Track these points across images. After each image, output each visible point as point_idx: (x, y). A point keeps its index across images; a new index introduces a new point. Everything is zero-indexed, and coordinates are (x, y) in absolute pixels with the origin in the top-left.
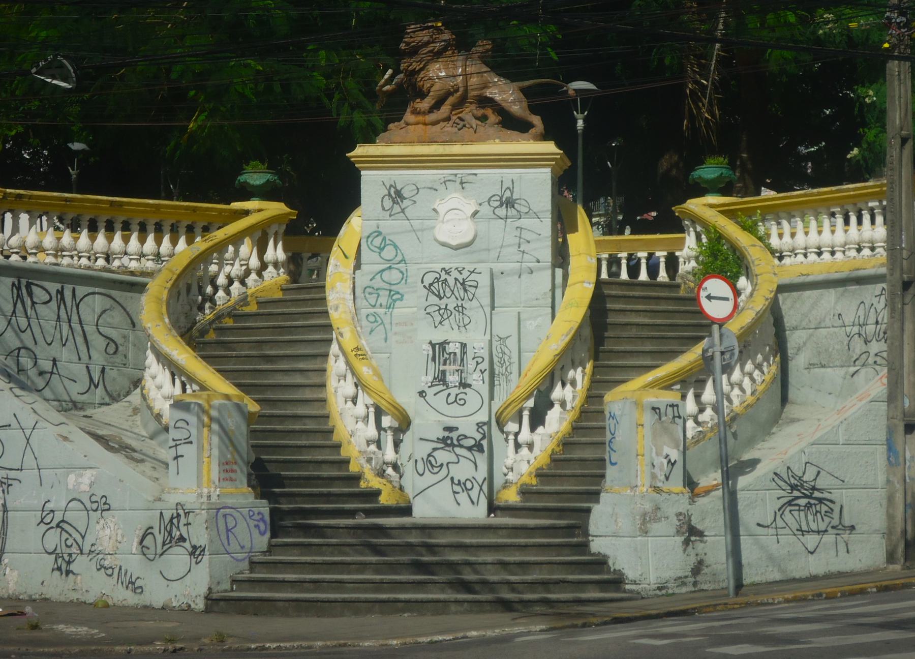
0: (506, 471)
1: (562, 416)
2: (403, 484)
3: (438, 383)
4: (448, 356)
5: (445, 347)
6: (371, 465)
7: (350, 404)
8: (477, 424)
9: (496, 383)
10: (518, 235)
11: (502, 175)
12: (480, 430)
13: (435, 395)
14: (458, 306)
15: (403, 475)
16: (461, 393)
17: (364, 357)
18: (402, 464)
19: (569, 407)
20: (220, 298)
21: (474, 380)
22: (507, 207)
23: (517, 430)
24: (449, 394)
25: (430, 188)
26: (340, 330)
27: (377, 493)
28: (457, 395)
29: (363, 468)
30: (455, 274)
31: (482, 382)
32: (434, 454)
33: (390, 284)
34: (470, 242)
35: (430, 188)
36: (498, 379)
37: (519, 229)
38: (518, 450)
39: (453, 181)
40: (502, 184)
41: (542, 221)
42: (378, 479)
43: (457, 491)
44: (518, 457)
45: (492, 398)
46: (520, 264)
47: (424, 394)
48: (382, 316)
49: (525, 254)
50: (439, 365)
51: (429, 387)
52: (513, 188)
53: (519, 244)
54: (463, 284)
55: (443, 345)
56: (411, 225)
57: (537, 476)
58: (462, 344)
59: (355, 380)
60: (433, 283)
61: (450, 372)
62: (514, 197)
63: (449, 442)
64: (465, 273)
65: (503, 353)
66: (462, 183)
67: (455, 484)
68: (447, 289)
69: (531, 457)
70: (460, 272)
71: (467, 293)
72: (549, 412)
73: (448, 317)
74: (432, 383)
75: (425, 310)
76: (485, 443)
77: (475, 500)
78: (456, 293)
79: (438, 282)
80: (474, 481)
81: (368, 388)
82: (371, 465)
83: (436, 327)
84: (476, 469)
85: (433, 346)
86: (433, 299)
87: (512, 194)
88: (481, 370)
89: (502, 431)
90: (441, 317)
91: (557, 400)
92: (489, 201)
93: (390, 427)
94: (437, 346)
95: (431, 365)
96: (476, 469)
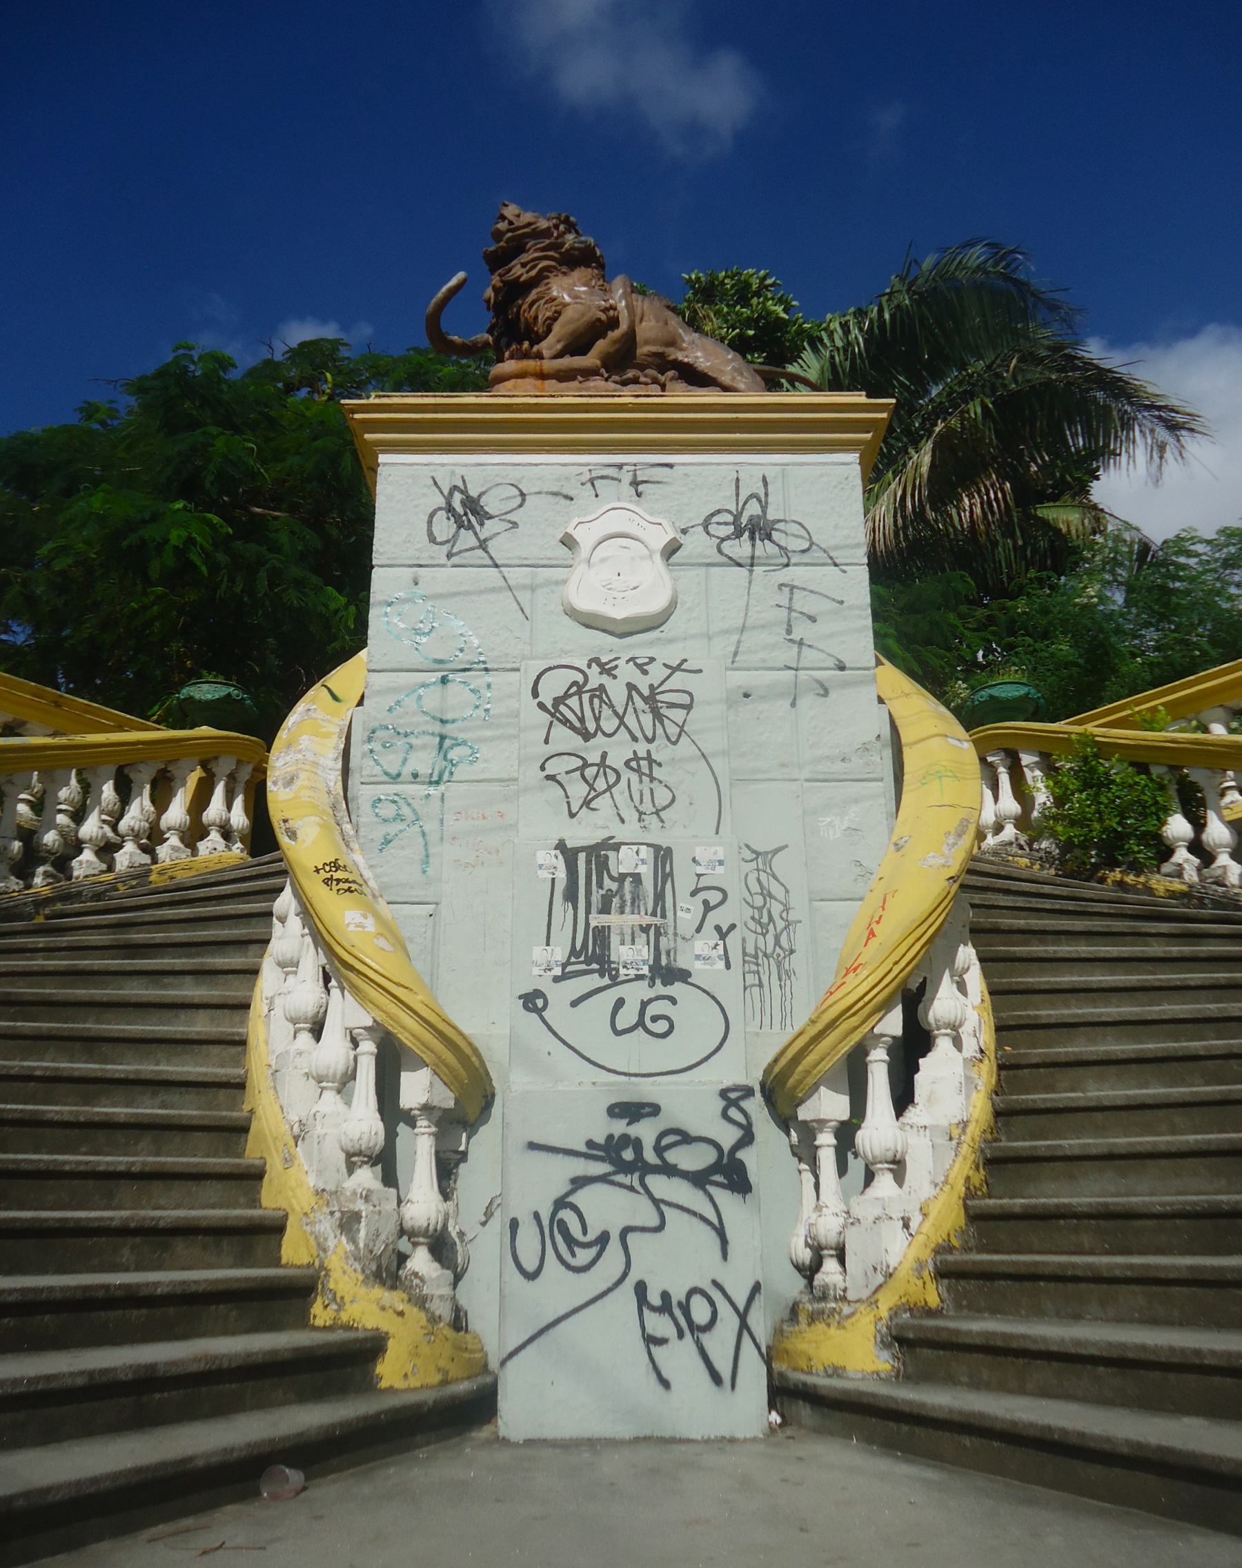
2: (463, 1302)
3: (583, 967)
4: (614, 886)
5: (607, 857)
6: (353, 1240)
7: (305, 1038)
8: (724, 1093)
10: (785, 603)
12: (734, 1113)
13: (574, 1004)
14: (636, 758)
15: (465, 1270)
17: (354, 886)
18: (461, 1234)
20: (81, 863)
21: (698, 957)
22: (752, 538)
23: (845, 1115)
24: (620, 1003)
26: (291, 824)
27: (373, 1347)
29: (325, 1250)
30: (627, 673)
31: (721, 964)
32: (578, 1199)
33: (442, 721)
37: (786, 590)
39: (613, 479)
40: (737, 487)
41: (844, 572)
42: (378, 1292)
43: (659, 1334)
44: (865, 1207)
46: (793, 672)
47: (540, 1003)
48: (415, 804)
49: (804, 648)
50: (588, 912)
51: (557, 979)
52: (766, 494)
53: (789, 625)
54: (651, 700)
55: (600, 853)
56: (504, 577)
57: (943, 1273)
58: (657, 848)
59: (323, 960)
60: (567, 695)
61: (622, 934)
62: (772, 515)
63: (628, 1155)
64: (657, 673)
65: (767, 895)
66: (635, 483)
67: (653, 1309)
68: (607, 712)
72: (916, 1076)
73: (609, 788)
74: (564, 966)
75: (543, 768)
78: (630, 720)
79: (579, 693)
80: (716, 1295)
81: (359, 973)
82: (353, 1240)
83: (572, 815)
85: (569, 854)
86: (564, 738)
87: (764, 509)
89: (785, 1121)
93: (427, 1108)
94: (582, 857)
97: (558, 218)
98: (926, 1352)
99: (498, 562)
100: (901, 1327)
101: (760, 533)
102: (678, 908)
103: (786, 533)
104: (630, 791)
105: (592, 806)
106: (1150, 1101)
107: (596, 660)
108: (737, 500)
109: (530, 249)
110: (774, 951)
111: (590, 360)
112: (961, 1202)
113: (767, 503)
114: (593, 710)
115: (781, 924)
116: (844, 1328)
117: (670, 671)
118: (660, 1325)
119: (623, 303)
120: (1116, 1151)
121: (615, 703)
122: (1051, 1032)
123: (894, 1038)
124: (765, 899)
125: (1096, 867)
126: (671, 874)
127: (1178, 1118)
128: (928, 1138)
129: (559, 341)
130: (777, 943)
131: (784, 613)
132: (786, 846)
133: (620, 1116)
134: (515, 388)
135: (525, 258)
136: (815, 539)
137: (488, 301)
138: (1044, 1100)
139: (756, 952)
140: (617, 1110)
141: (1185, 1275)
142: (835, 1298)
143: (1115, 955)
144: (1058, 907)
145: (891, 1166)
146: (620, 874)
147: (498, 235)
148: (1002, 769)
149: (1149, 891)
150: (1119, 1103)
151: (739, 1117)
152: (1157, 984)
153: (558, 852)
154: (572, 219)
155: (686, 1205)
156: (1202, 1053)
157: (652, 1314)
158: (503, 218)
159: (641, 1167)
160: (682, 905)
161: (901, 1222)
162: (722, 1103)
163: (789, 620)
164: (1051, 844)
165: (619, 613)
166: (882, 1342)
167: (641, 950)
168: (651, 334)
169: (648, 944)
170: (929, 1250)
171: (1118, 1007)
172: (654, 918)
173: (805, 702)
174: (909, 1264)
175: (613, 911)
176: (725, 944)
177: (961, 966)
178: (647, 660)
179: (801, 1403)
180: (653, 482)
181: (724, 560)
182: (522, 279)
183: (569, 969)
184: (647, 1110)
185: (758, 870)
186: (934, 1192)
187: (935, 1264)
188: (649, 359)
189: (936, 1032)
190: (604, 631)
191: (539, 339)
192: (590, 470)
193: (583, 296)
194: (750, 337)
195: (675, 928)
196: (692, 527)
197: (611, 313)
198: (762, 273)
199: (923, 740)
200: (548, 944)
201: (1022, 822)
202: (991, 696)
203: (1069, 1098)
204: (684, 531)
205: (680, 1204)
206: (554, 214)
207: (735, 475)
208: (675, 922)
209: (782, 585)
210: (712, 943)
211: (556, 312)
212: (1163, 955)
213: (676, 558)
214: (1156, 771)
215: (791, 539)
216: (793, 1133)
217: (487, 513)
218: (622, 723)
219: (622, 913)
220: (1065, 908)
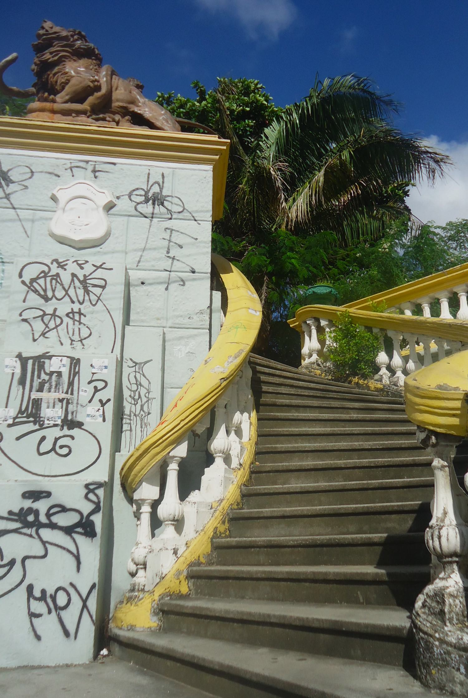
0: (133, 568)
1: (227, 475)
3: (25, 419)
4: (47, 378)
5: (44, 362)
8: (87, 486)
9: (125, 427)
10: (168, 238)
11: (149, 168)
12: (91, 496)
13: (18, 439)
14: (73, 312)
16: (64, 436)
19: (235, 463)
21: (88, 415)
22: (154, 204)
23: (156, 497)
24: (43, 439)
25: (50, 173)
28: (56, 440)
30: (72, 268)
31: (101, 419)
34: (101, 238)
35: (50, 173)
36: (128, 421)
37: (169, 231)
38: (156, 532)
39: (83, 168)
40: (148, 177)
41: (199, 224)
43: (37, 612)
44: (157, 543)
45: (116, 447)
46: (169, 272)
50: (31, 391)
51: (9, 426)
52: (163, 182)
54: (84, 283)
57: (191, 576)
58: (72, 359)
60: (38, 278)
61: (48, 403)
62: (164, 193)
64: (88, 269)
66: (94, 171)
67: (36, 599)
68: (59, 287)
69: (179, 541)
70: (81, 266)
71: (88, 294)
72: (202, 477)
73: (56, 327)
74: (14, 419)
76: (97, 519)
77: (71, 629)
78: (71, 292)
79: (45, 277)
83: (35, 340)
84: (78, 569)
85: (23, 361)
86: (34, 299)
87: (161, 189)
88: (101, 401)
89: (131, 500)
90: (44, 326)
91: (220, 452)
92: (130, 195)
94: (30, 362)
95: (16, 390)
96: (78, 569)
97: (74, 32)
98: (172, 617)
99: (15, 206)
100: (162, 605)
101: (158, 202)
102: (80, 390)
103: (172, 203)
104: (67, 329)
105: (46, 336)
106: (311, 490)
107: (56, 261)
108: (148, 184)
109: (55, 45)
110: (140, 413)
111: (86, 106)
112: (210, 540)
113: (163, 187)
114: (52, 286)
115: (144, 399)
116: (137, 605)
117: (96, 268)
118: (38, 607)
119: (105, 79)
120: (286, 514)
121: (64, 283)
122: (283, 455)
123: (182, 458)
124: (138, 387)
125: (348, 376)
126: (78, 372)
127: (323, 497)
128: (196, 508)
129: (67, 95)
130: (142, 409)
131: (166, 243)
132: (152, 360)
133: (29, 498)
134: (37, 116)
135: (53, 49)
136: (186, 207)
137: (33, 70)
138: (264, 489)
139: (130, 413)
140: (27, 495)
141: (285, 576)
142: (138, 590)
143: (326, 418)
144: (312, 394)
145: (173, 523)
146: (51, 372)
147: (39, 36)
148: (313, 327)
149: (368, 388)
150: (298, 490)
151: (94, 498)
152: (339, 432)
153: (17, 359)
154: (83, 33)
155: (60, 544)
156: (343, 466)
157: (35, 601)
158: (43, 28)
159: (38, 525)
160: (83, 388)
161: (173, 551)
162: (86, 491)
163: (169, 247)
164: (331, 364)
165: (76, 237)
166: (154, 612)
167: (57, 411)
168: (120, 97)
169: (62, 408)
170: (185, 565)
171: (320, 443)
172: (66, 395)
173: (172, 287)
174: (174, 571)
175: (45, 390)
176: (103, 409)
177: (236, 422)
178: (84, 262)
179: (116, 644)
180: (104, 172)
181: (138, 214)
182: (49, 61)
183: (17, 420)
184: (44, 494)
185: (135, 372)
186: (195, 536)
187: (188, 572)
188: (118, 109)
189: (215, 455)
190: (70, 246)
191: (56, 93)
192: (71, 163)
193: (82, 73)
194: (247, 111)
195: (78, 400)
196: (123, 196)
197: (96, 83)
198: (256, 81)
199: (238, 310)
200: (6, 407)
201: (320, 353)
202: (314, 292)
203: (276, 488)
204: (118, 198)
205: (57, 543)
206: (71, 29)
207: (148, 171)
208: (78, 397)
209: (167, 228)
210: (97, 409)
211: (67, 80)
212: (349, 418)
213: (113, 211)
214: (375, 330)
215: (174, 206)
216: (134, 506)
217: (11, 180)
218: (67, 293)
219: (50, 392)
220: (315, 395)
